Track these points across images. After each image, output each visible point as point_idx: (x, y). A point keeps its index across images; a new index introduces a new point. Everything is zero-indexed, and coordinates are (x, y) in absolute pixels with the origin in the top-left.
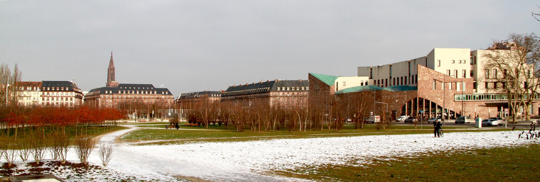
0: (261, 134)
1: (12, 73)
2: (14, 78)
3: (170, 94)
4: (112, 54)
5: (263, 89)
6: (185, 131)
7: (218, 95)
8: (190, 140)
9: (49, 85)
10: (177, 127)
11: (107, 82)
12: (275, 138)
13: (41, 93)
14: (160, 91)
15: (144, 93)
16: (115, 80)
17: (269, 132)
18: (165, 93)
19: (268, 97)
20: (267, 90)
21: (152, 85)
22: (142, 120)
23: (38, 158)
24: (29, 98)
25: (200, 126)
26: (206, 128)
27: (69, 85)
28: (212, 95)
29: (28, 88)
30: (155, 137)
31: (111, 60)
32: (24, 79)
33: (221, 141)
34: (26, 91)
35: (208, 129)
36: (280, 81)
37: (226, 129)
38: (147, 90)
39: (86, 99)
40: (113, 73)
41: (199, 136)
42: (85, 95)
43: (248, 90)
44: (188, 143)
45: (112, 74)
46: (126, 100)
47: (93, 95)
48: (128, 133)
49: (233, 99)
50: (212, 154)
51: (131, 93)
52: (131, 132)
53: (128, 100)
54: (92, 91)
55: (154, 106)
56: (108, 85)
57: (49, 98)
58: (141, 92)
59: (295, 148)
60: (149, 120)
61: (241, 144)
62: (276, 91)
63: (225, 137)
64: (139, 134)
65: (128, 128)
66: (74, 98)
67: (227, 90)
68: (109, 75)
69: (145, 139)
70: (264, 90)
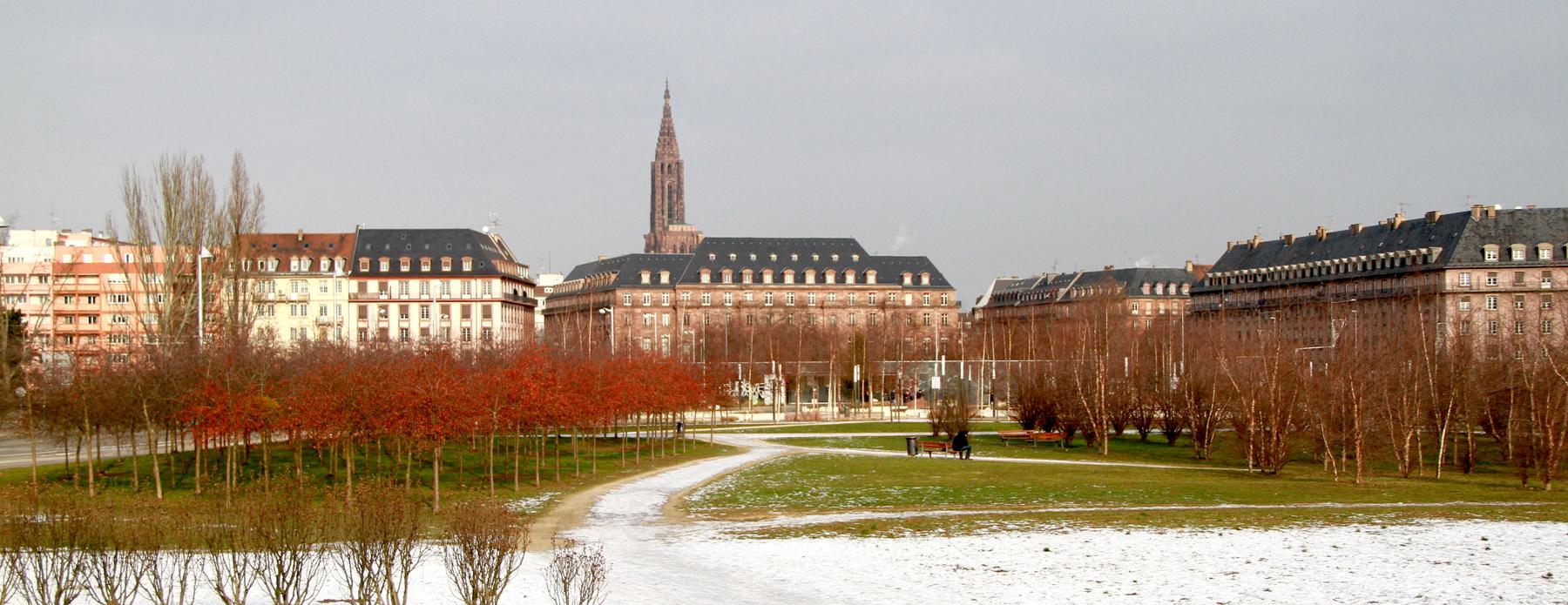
0: (1368, 493)
1: (222, 197)
2: (233, 217)
3: (939, 282)
4: (667, 96)
5: (1408, 253)
6: (995, 469)
7: (1172, 289)
8: (1007, 517)
9: (387, 247)
10: (960, 443)
11: (647, 230)
12: (1434, 513)
13: (352, 286)
14: (891, 270)
15: (821, 279)
16: (687, 220)
17: (1415, 483)
18: (917, 281)
19: (1435, 296)
20: (1425, 258)
21: (853, 241)
22: (805, 410)
23: (290, 596)
24: (299, 307)
25: (1075, 442)
26: (1100, 456)
27: (476, 246)
28: (1146, 289)
29: (294, 263)
30: (843, 500)
31: (662, 128)
32: (275, 221)
33: (1152, 525)
34: (285, 276)
35: (1108, 458)
36: (1497, 212)
37: (1199, 459)
38: (832, 265)
39: (552, 310)
40: (675, 188)
41: (1056, 497)
42: (549, 291)
43: (1327, 262)
44: (995, 527)
45: (670, 192)
46: (734, 312)
47: (585, 293)
48: (729, 477)
49: (1247, 309)
50: (1088, 591)
51: (758, 279)
52: (743, 473)
53: (744, 313)
54: (578, 272)
55: (864, 345)
56: (653, 242)
57: (385, 308)
58: (824, 274)
59: (1518, 572)
60: (841, 412)
61: (1249, 541)
62: (1478, 263)
63: (1179, 503)
64: (776, 479)
65: (732, 450)
66: (497, 308)
67: (1219, 263)
68: (658, 197)
69: (799, 508)
70: (1408, 262)
